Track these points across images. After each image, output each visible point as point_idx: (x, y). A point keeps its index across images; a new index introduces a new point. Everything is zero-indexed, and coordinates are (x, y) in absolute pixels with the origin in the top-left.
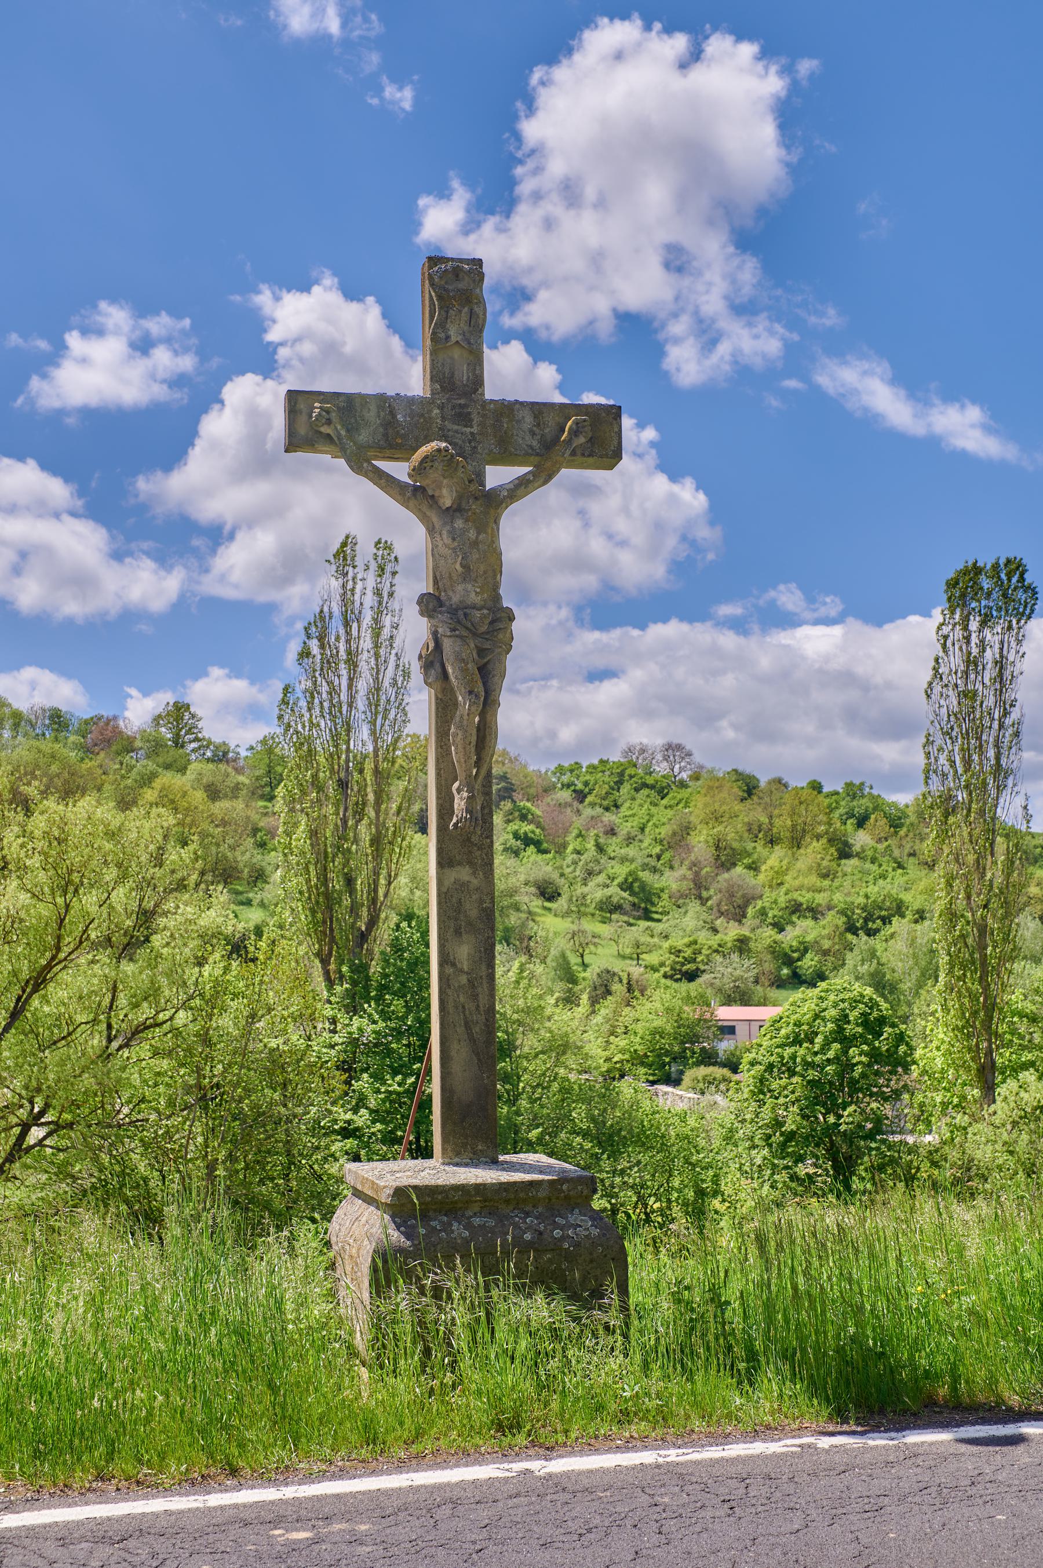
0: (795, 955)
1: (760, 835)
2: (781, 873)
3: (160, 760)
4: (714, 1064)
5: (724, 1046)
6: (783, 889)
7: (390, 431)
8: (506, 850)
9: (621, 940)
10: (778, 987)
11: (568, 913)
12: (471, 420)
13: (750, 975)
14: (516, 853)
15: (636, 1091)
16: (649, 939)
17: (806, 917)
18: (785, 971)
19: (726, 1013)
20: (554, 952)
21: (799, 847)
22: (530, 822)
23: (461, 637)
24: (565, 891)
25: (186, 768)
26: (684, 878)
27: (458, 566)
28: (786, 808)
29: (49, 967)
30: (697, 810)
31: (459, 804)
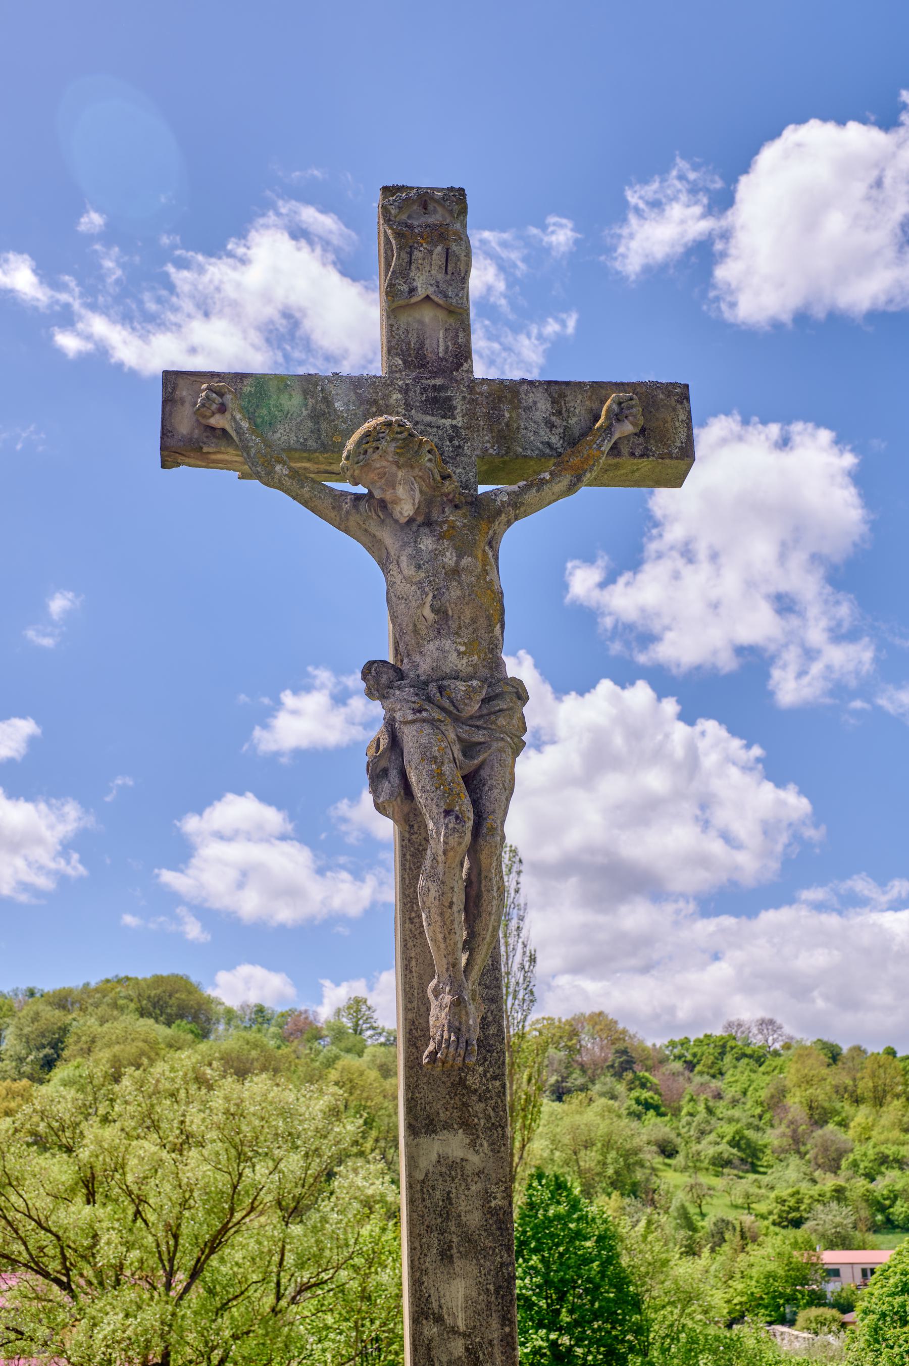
0: (887, 1202)
1: (846, 1096)
2: (867, 1129)
3: (343, 1045)
4: (824, 1305)
5: (832, 1288)
6: (871, 1143)
7: (324, 426)
8: (629, 1114)
9: (733, 1192)
10: (875, 1232)
11: (685, 1169)
12: (452, 408)
13: (849, 1221)
14: (639, 1116)
15: (759, 1342)
16: (757, 1191)
17: (893, 1168)
18: (879, 1217)
19: (831, 1257)
20: (675, 1204)
21: (881, 1106)
22: (649, 1089)
23: (431, 722)
24: (682, 1149)
25: (362, 1052)
26: (783, 1135)
27: (427, 612)
28: (867, 1072)
29: (225, 1229)
30: (790, 1076)
31: (438, 1017)
